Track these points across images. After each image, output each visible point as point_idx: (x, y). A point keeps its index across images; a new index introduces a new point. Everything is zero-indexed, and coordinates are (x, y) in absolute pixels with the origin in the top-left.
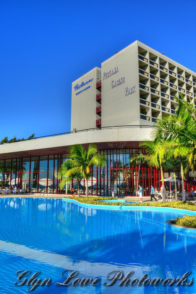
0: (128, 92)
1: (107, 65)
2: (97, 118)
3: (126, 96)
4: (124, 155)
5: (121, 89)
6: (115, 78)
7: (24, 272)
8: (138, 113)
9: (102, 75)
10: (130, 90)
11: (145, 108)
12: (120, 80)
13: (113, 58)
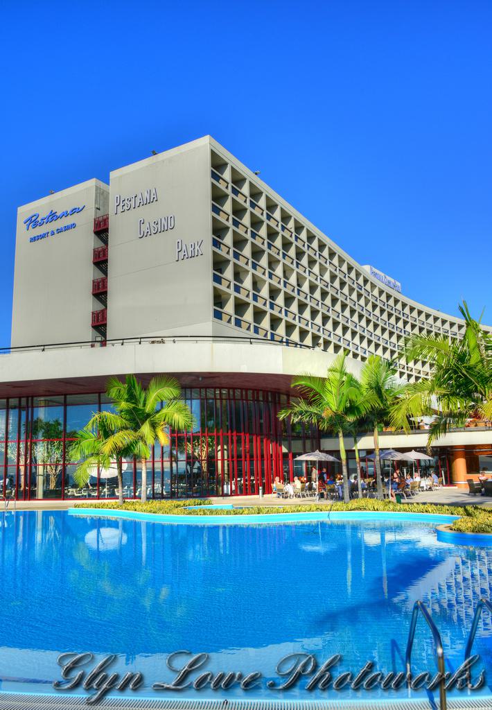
0: (183, 254)
1: (128, 178)
2: (93, 306)
3: (178, 261)
4: (189, 402)
5: (165, 243)
6: (150, 214)
7: (77, 657)
8: (210, 307)
9: (112, 203)
11: (221, 293)
12: (163, 220)
13: (409, 299)
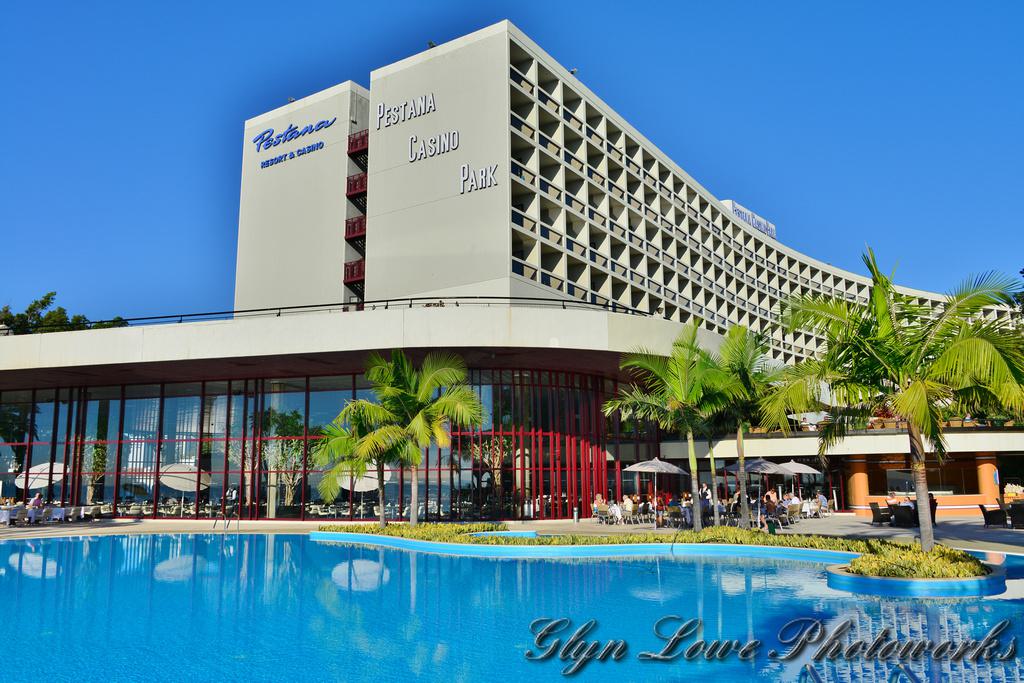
10: (480, 177)
